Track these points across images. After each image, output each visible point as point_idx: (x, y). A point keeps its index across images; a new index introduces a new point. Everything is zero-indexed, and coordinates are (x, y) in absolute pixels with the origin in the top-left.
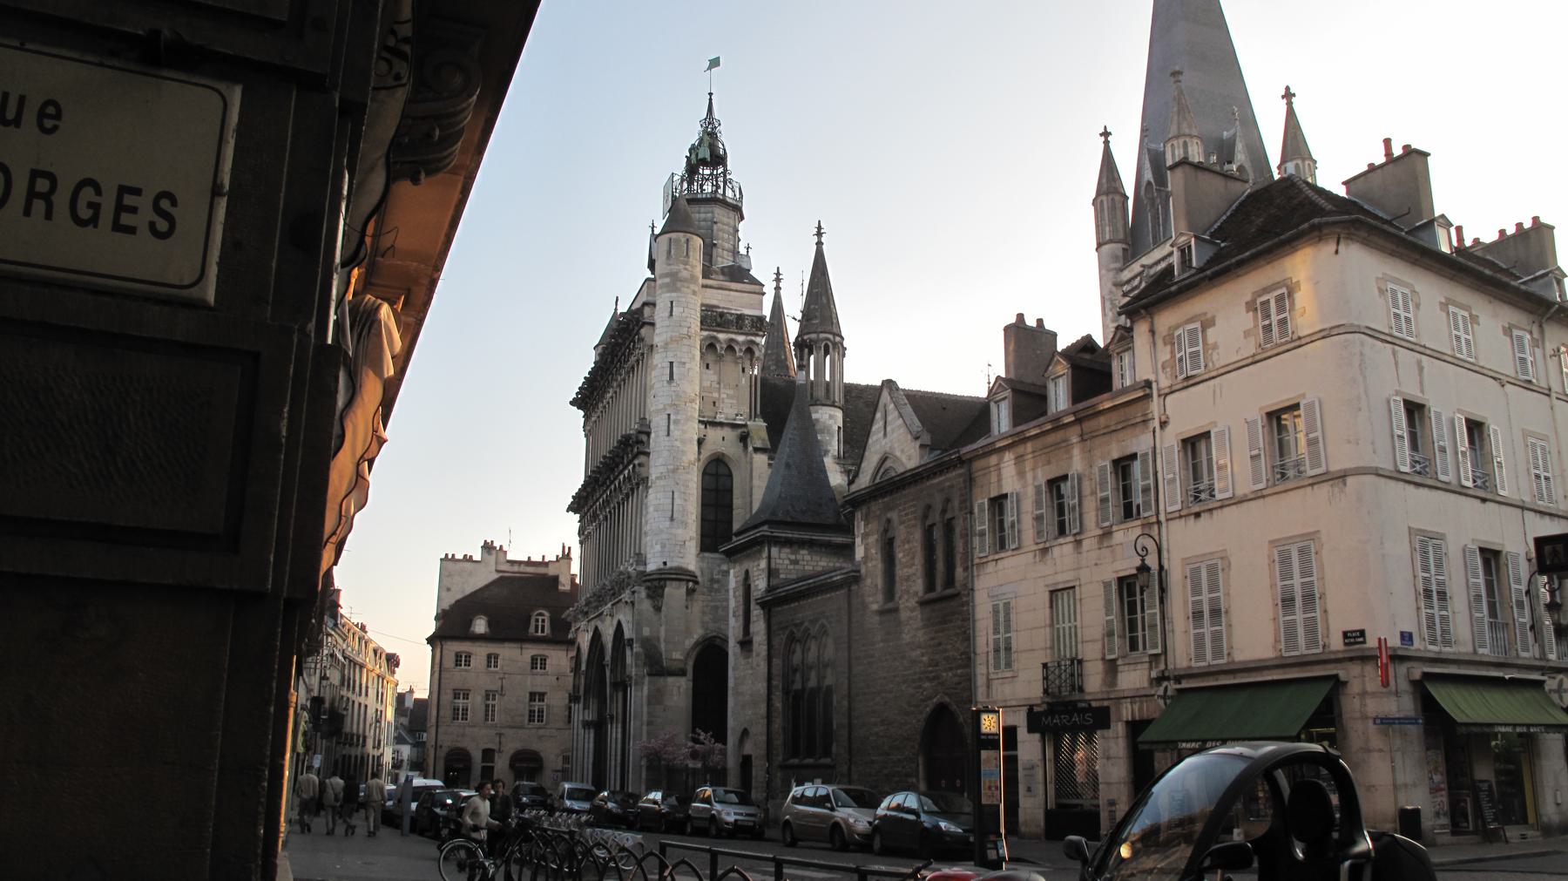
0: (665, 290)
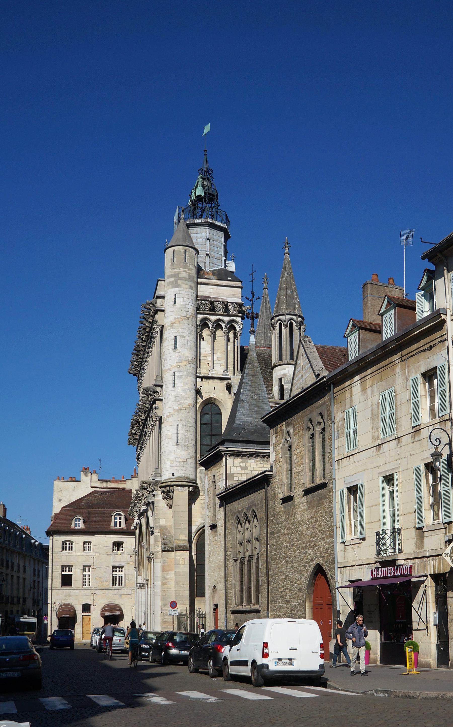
0: (171, 286)
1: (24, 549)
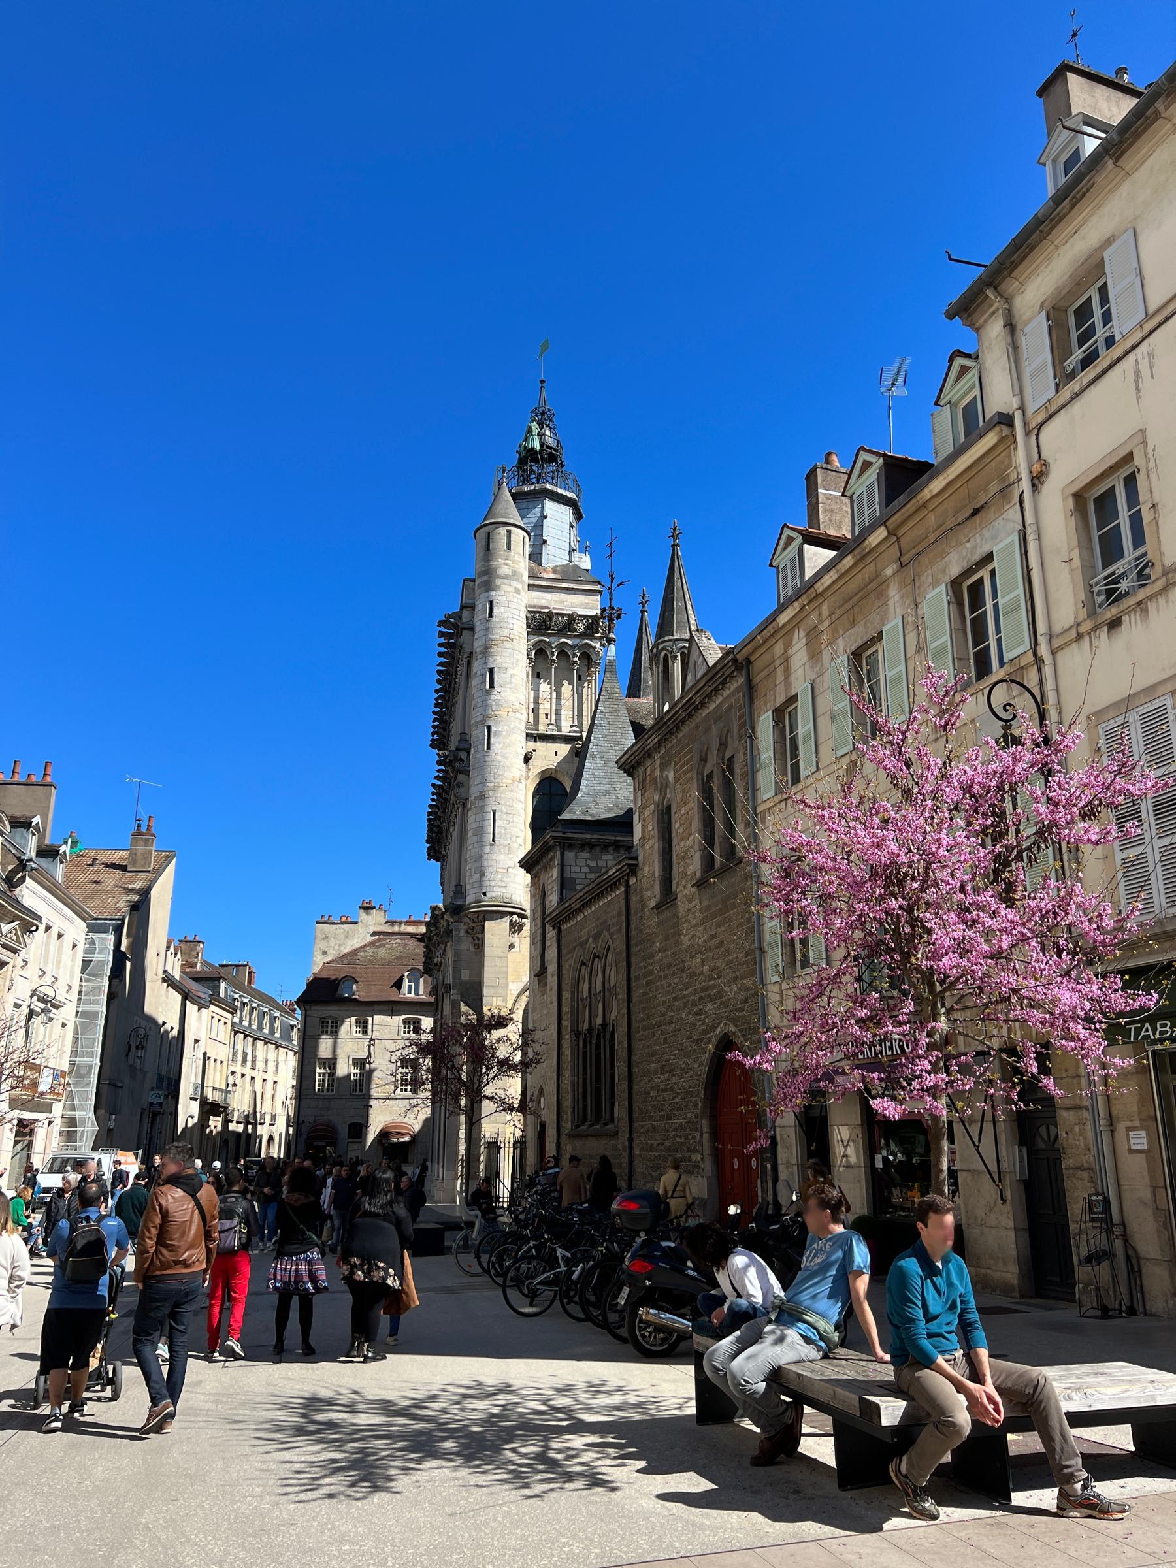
1: (277, 1035)
